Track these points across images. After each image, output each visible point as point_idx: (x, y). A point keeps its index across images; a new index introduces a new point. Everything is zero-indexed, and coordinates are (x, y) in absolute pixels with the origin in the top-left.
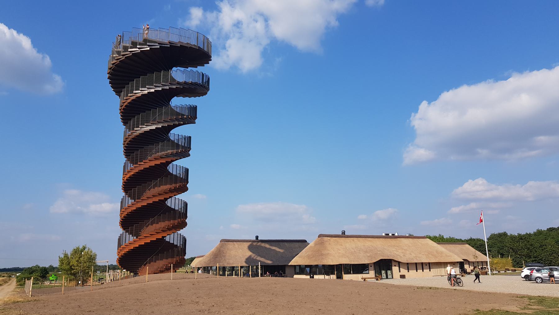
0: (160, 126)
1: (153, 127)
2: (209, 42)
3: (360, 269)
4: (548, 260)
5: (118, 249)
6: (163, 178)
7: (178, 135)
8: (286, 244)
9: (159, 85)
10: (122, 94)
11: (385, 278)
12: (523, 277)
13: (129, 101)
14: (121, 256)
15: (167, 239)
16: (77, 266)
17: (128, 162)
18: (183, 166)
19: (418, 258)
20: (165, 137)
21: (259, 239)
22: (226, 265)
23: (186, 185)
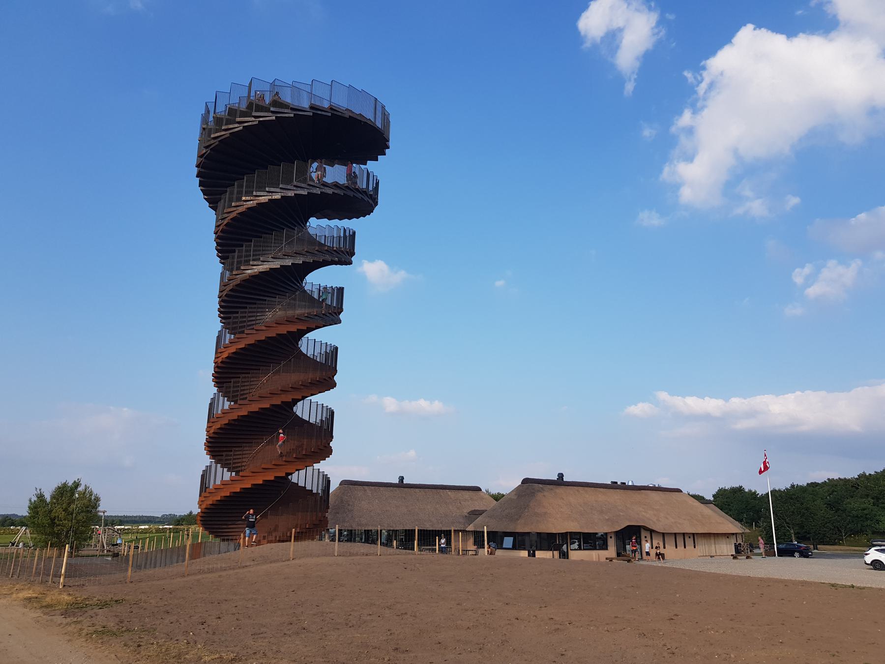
0: (288, 262)
1: (276, 264)
2: (386, 113)
3: (591, 541)
4: (819, 533)
5: (200, 495)
6: (290, 360)
7: (315, 342)
8: (449, 493)
9: (303, 185)
10: (220, 205)
11: (511, 547)
12: (869, 563)
13: (241, 209)
14: (206, 508)
15: (294, 478)
16: (65, 520)
18: (326, 343)
19: (679, 525)
21: (405, 482)
22: (355, 527)
23: (333, 377)
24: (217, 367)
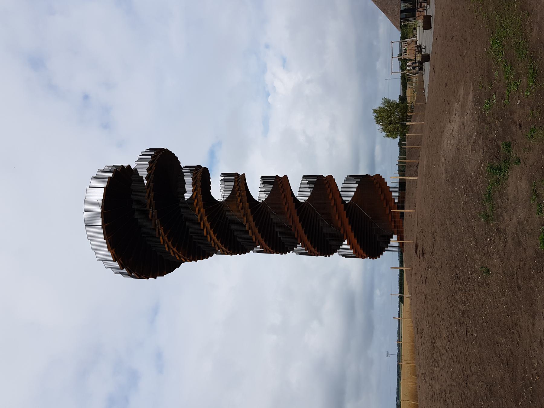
7: (260, 192)
17: (296, 250)
20: (155, 223)
23: (325, 177)
24: (321, 255)
